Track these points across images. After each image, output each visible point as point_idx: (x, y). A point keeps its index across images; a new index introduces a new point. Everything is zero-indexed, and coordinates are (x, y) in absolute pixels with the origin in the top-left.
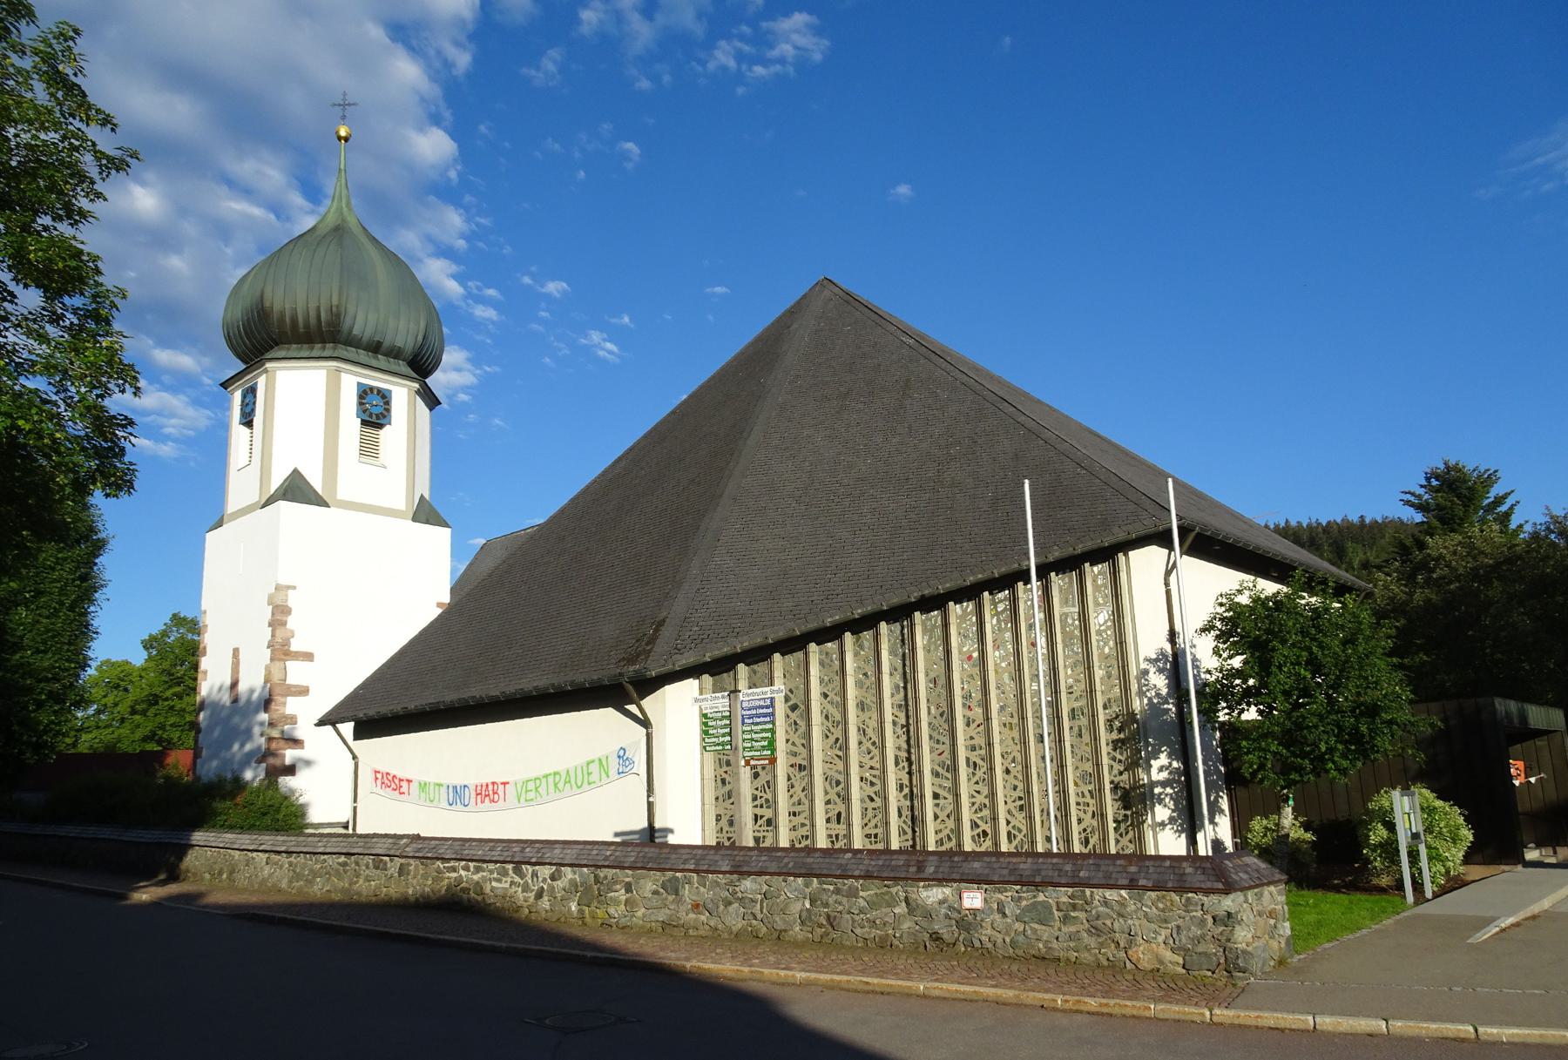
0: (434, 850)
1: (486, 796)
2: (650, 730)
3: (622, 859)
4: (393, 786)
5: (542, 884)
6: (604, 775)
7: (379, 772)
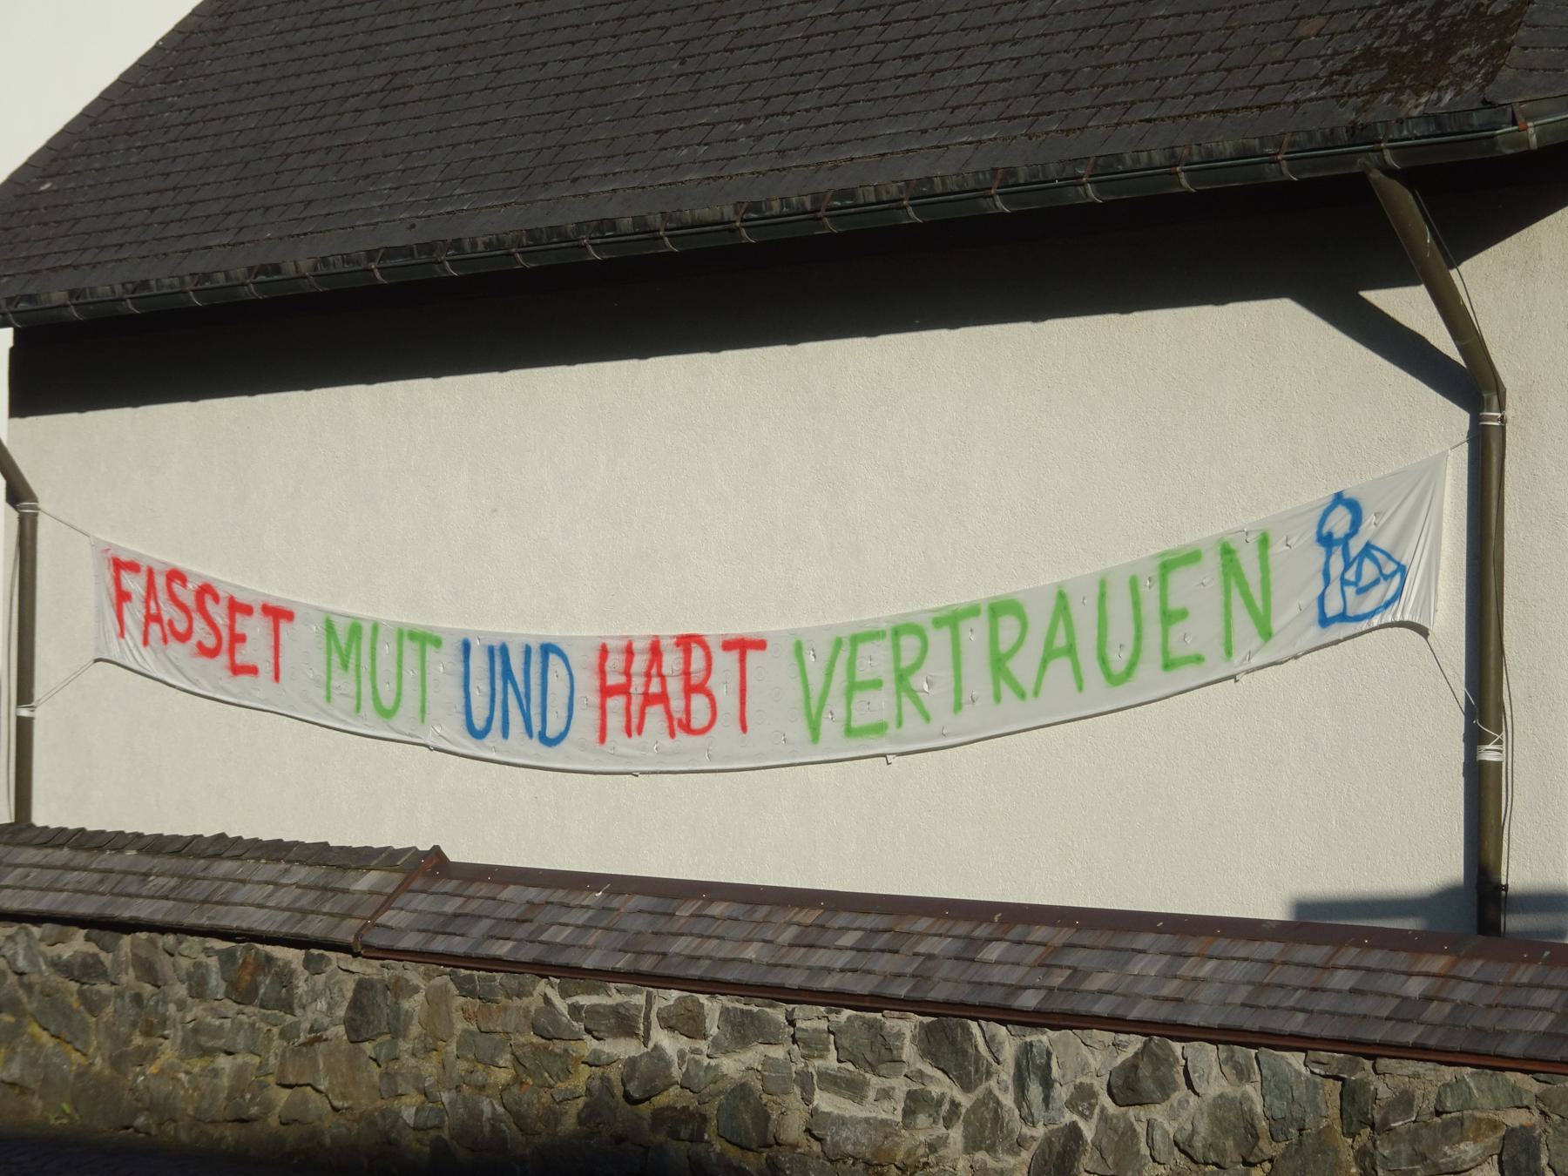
0: (524, 931)
1: (649, 699)
2: (1492, 417)
3: (1488, 1021)
4: (200, 629)
5: (1069, 1117)
6: (1243, 624)
7: (133, 567)
